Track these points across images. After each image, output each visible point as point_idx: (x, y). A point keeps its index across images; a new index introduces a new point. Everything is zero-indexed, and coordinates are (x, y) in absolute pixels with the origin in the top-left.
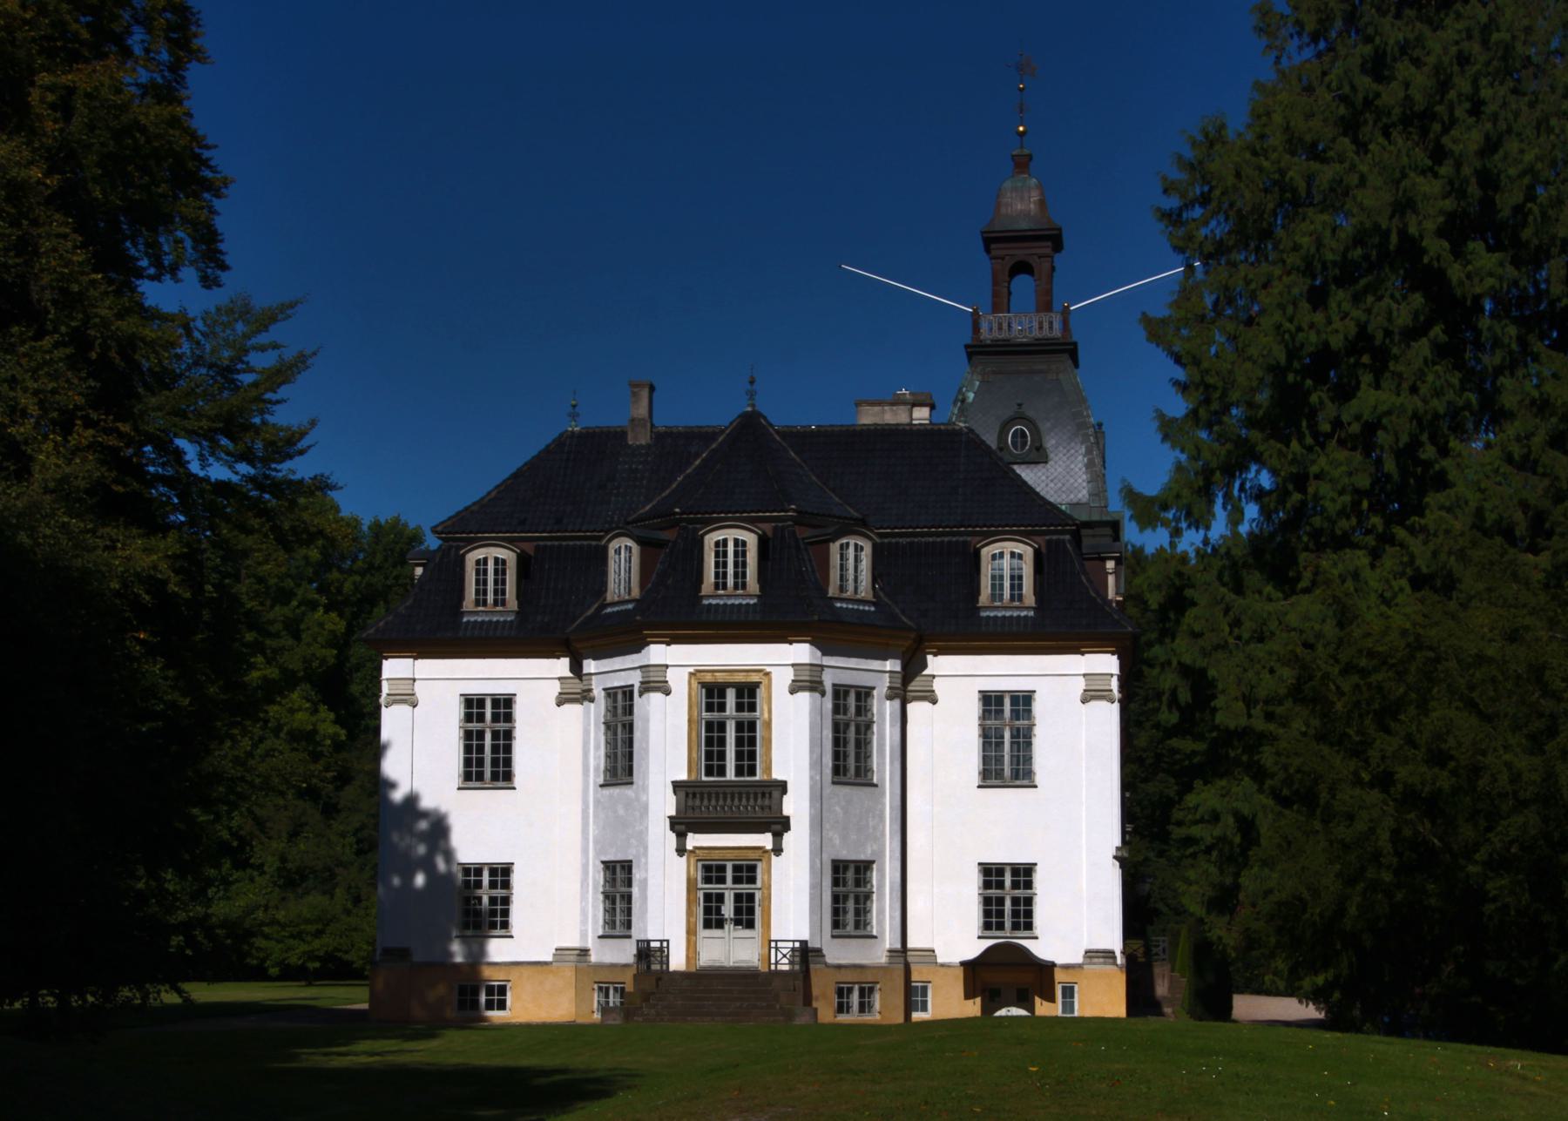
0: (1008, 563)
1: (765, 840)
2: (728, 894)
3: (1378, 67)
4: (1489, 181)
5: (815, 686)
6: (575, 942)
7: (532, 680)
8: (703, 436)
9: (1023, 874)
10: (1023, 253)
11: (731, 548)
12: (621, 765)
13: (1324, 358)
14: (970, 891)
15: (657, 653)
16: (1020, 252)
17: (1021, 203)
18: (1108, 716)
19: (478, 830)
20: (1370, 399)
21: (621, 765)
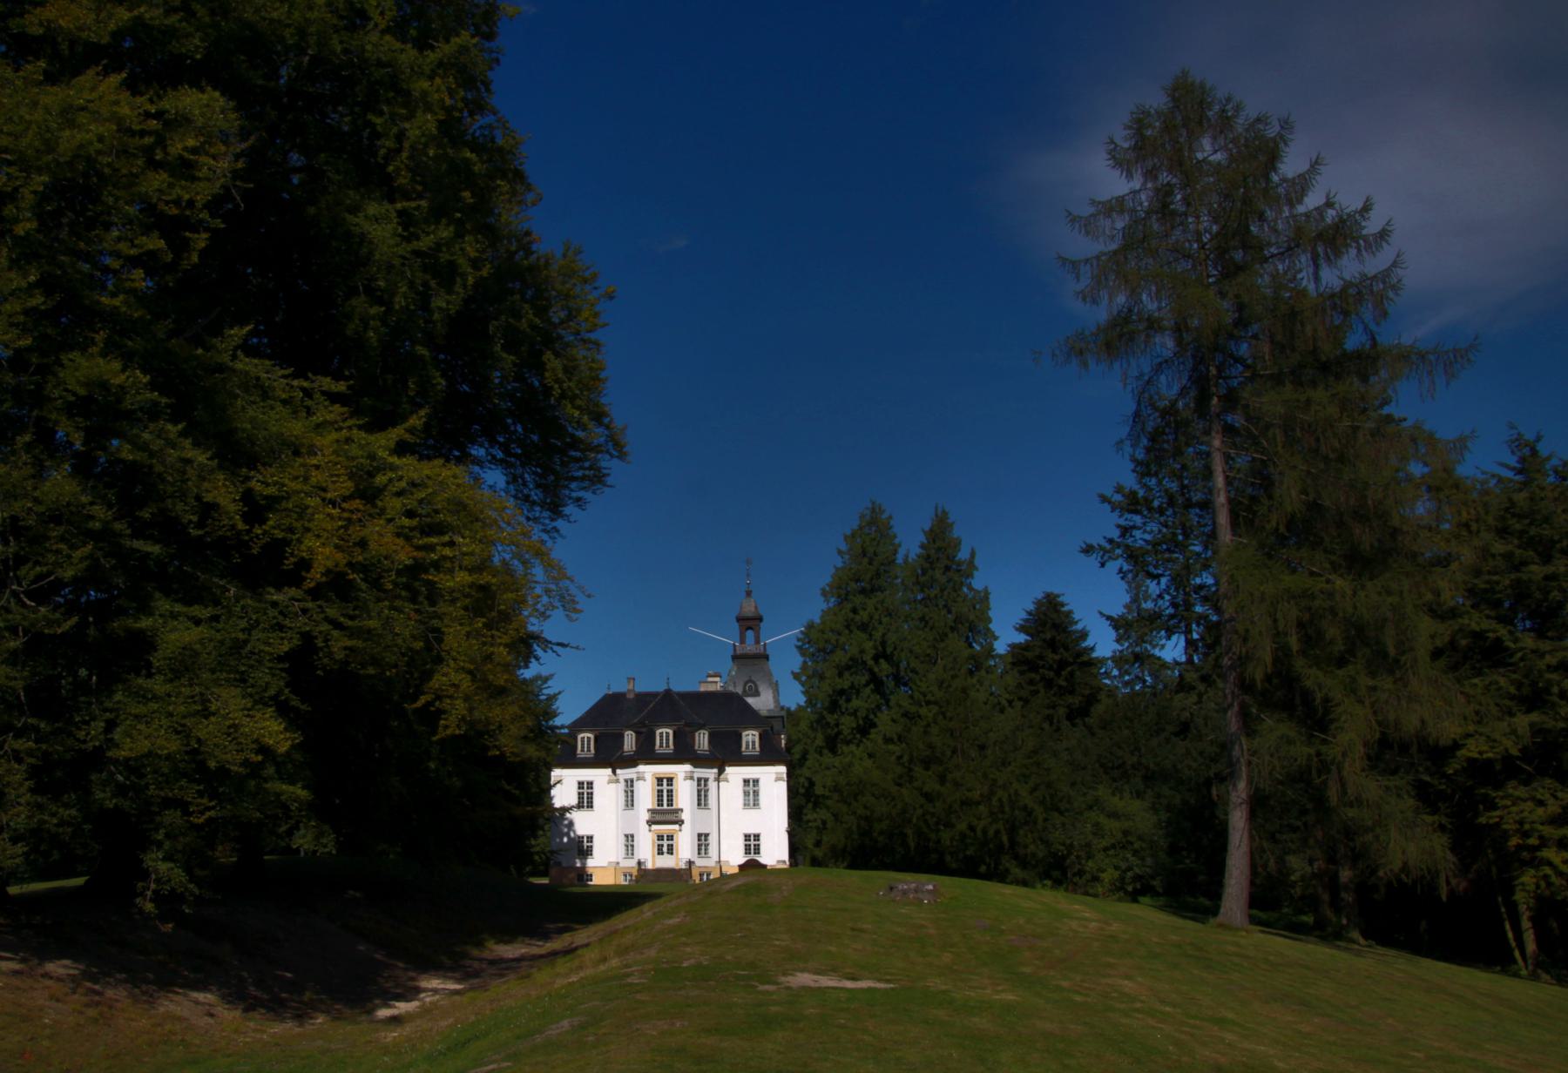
0: (750, 738)
1: (676, 827)
2: (665, 845)
3: (854, 611)
4: (883, 643)
5: (692, 778)
6: (614, 859)
7: (600, 776)
8: (654, 695)
9: (757, 837)
10: (750, 623)
11: (664, 736)
12: (630, 801)
13: (842, 692)
14: (741, 843)
15: (641, 768)
16: (750, 623)
17: (749, 609)
18: (783, 786)
19: (583, 823)
20: (855, 703)
21: (630, 801)
